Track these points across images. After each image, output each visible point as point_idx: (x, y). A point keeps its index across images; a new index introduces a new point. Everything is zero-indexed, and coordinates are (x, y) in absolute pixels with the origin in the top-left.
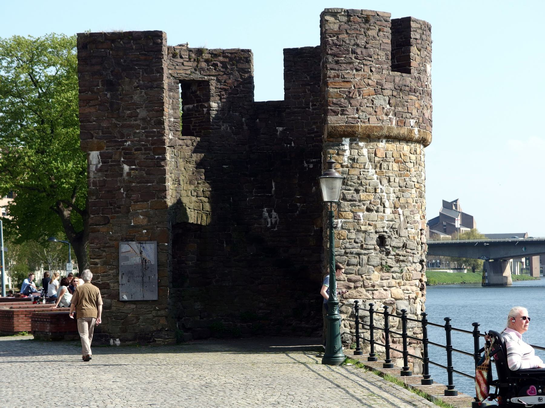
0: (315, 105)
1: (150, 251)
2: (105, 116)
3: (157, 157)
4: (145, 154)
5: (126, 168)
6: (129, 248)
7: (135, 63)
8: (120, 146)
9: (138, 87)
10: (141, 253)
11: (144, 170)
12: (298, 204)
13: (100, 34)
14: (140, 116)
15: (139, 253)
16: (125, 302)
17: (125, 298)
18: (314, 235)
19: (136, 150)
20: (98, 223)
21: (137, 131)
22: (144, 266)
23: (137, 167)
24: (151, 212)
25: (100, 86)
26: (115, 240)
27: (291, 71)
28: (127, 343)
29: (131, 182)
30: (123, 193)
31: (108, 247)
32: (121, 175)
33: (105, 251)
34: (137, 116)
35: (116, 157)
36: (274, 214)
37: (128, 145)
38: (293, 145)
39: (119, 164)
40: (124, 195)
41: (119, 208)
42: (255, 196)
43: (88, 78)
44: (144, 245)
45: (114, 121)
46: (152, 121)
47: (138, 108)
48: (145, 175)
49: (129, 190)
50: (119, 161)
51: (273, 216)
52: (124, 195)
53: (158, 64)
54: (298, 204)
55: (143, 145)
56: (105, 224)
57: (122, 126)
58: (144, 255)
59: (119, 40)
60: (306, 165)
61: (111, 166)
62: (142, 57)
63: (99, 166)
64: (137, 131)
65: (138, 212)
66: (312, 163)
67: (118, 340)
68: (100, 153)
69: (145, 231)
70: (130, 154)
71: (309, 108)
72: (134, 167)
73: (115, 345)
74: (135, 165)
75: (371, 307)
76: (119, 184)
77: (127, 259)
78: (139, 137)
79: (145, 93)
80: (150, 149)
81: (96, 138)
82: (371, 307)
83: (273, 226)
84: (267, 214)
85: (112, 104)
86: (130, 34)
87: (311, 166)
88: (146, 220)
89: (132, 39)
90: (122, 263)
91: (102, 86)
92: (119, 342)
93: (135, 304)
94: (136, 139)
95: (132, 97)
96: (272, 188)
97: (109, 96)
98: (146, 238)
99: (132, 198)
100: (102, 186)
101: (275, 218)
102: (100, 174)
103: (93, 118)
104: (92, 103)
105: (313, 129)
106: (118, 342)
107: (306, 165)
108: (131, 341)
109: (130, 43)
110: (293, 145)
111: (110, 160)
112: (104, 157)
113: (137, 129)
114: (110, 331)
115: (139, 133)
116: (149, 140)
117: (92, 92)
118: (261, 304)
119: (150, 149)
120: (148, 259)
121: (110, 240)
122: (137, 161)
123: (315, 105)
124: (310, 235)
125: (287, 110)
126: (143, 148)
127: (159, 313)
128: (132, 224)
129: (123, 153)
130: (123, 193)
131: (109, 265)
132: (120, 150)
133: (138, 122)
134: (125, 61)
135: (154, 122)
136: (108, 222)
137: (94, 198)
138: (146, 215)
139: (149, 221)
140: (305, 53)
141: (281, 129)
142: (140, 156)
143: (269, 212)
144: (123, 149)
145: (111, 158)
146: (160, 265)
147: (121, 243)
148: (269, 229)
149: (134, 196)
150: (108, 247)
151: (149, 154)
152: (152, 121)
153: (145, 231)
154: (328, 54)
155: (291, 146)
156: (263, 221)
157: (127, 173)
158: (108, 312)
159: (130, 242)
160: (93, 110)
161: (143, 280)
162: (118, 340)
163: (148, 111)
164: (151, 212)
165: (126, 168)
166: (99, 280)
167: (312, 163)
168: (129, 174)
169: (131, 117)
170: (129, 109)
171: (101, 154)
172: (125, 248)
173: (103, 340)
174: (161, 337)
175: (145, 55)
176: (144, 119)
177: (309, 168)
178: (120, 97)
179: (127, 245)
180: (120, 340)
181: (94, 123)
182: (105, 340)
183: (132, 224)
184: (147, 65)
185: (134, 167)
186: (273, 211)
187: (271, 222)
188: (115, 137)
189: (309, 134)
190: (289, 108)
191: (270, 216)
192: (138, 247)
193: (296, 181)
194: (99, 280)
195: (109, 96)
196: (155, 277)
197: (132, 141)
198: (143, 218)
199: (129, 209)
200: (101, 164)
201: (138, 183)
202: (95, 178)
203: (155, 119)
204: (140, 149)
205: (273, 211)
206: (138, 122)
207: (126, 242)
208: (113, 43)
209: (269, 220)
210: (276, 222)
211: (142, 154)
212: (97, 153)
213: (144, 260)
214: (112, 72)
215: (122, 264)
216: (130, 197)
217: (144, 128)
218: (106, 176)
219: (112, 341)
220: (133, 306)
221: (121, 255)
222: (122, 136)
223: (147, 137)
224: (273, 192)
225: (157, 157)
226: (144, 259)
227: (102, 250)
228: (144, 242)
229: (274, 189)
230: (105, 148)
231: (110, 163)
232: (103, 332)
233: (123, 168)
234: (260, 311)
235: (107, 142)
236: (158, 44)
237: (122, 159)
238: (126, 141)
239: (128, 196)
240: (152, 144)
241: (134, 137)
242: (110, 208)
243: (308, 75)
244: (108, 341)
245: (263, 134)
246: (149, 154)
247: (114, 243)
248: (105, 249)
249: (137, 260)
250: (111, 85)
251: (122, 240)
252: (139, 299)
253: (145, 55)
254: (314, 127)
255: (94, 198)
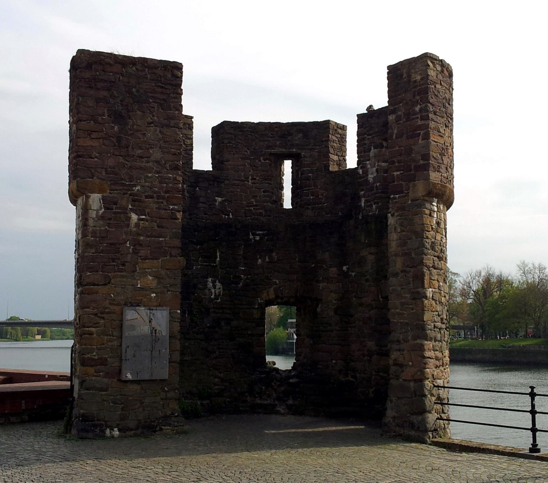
0: (255, 179)
1: (161, 319)
2: (110, 153)
3: (171, 207)
4: (158, 203)
5: (134, 217)
6: (136, 315)
7: (150, 95)
8: (129, 190)
9: (152, 123)
10: (150, 322)
11: (156, 222)
12: (242, 276)
13: (111, 55)
14: (152, 158)
15: (148, 321)
16: (126, 382)
17: (129, 376)
18: (258, 308)
19: (147, 197)
20: (96, 283)
21: (149, 175)
22: (154, 337)
23: (148, 217)
24: (163, 272)
25: (107, 116)
26: (117, 305)
27: (231, 143)
28: (128, 433)
29: (139, 235)
30: (130, 247)
31: (108, 313)
32: (128, 226)
33: (103, 318)
34: (149, 157)
35: (124, 203)
36: (218, 285)
37: (138, 190)
38: (231, 216)
39: (125, 211)
40: (131, 250)
41: (123, 265)
42: (201, 265)
43: (91, 105)
44: (154, 312)
45: (121, 159)
46: (168, 165)
47: (151, 148)
48: (156, 227)
49: (137, 244)
50: (126, 209)
51: (217, 287)
52: (131, 250)
53: (176, 100)
54: (242, 276)
55: (155, 192)
56: (105, 285)
57: (131, 168)
58: (154, 323)
59: (131, 66)
60: (251, 237)
61: (115, 213)
62: (159, 90)
63: (101, 212)
64: (149, 175)
65: (146, 272)
66: (258, 235)
67: (116, 429)
68: (103, 196)
69: (155, 295)
70: (140, 201)
71: (248, 182)
72: (144, 217)
73: (113, 437)
74: (145, 215)
75: (532, 390)
76: (124, 237)
77: (133, 327)
78: (151, 182)
79: (160, 131)
80: (163, 198)
81: (98, 178)
82: (532, 390)
83: (216, 297)
84: (212, 284)
85: (119, 139)
86: (143, 61)
87: (258, 238)
88: (156, 281)
89: (146, 67)
90: (126, 333)
91: (108, 116)
92: (118, 433)
93: (139, 384)
94: (147, 184)
95: (144, 134)
96: (217, 258)
97: (116, 128)
98: (155, 304)
99: (139, 255)
100: (104, 237)
101: (220, 289)
102: (101, 222)
103: (94, 153)
104: (94, 135)
105: (252, 203)
106: (116, 433)
107: (251, 237)
108: (132, 430)
109: (144, 71)
110: (231, 216)
111: (114, 206)
112: (107, 203)
113: (150, 173)
114: (106, 419)
115: (150, 177)
116: (163, 187)
117: (96, 121)
118: (216, 380)
119: (163, 198)
120: (158, 328)
121: (111, 304)
122: (147, 211)
123: (255, 179)
124: (254, 308)
125: (226, 182)
126: (155, 195)
127: (169, 395)
128: (139, 286)
129: (130, 199)
130: (130, 247)
131: (107, 335)
132: (127, 196)
133: (151, 164)
134: (138, 91)
135: (170, 166)
136: (109, 283)
137: (93, 251)
138: (157, 277)
139: (159, 283)
140: (245, 127)
141: (219, 199)
142: (151, 204)
143: (214, 282)
144: (130, 195)
145: (115, 203)
146: (172, 337)
147: (126, 308)
148: (212, 300)
149: (143, 253)
150: (108, 313)
151: (162, 203)
152: (168, 165)
153: (155, 295)
154: (429, 103)
155: (229, 218)
156: (207, 291)
157: (136, 223)
158: (105, 395)
159: (137, 308)
160: (96, 143)
161: (152, 355)
162: (116, 429)
163: (163, 152)
164: (163, 272)
165: (134, 217)
166: (95, 354)
167: (258, 235)
168: (137, 225)
169: (141, 157)
170: (140, 148)
171: (104, 198)
172: (130, 315)
173: (98, 430)
174: (170, 425)
175: (162, 87)
176: (158, 162)
177: (255, 241)
178: (130, 132)
179: (133, 311)
180: (119, 430)
181: (96, 159)
182: (100, 430)
183: (139, 286)
184: (164, 99)
185: (144, 217)
186: (217, 281)
187: (215, 293)
188: (122, 179)
189: (247, 206)
190: (227, 180)
191: (214, 287)
192: (147, 314)
193: (241, 253)
194: (95, 354)
195: (116, 128)
196: (166, 351)
197: (142, 186)
198: (153, 280)
199: (136, 267)
200: (103, 210)
201: (148, 236)
202: (94, 226)
203: (171, 163)
204: (152, 197)
205: (217, 281)
206: (151, 164)
207: (132, 308)
208: (124, 68)
209: (213, 291)
210: (220, 293)
211: (154, 202)
212: (100, 196)
213: (154, 331)
214: (121, 101)
215: (127, 334)
216: (138, 253)
217: (158, 172)
218: (109, 225)
219: (108, 431)
220: (136, 387)
221: (126, 324)
222: (131, 179)
223: (161, 182)
224: (217, 263)
225: (171, 207)
226: (153, 328)
227: (99, 317)
228: (155, 308)
229: (218, 259)
230: (108, 191)
231: (114, 210)
232: (98, 420)
233: (130, 218)
234: (216, 387)
235: (111, 184)
236: (178, 77)
237: (130, 207)
238: (135, 186)
239: (135, 252)
240: (166, 192)
241: (146, 182)
242: (112, 265)
243: (249, 150)
244: (103, 432)
245: (202, 203)
246: (162, 203)
247: (117, 308)
248: (104, 315)
249: (146, 329)
250: (119, 118)
251: (126, 304)
252: (147, 379)
253: (162, 87)
254: (252, 200)
255: (93, 251)
